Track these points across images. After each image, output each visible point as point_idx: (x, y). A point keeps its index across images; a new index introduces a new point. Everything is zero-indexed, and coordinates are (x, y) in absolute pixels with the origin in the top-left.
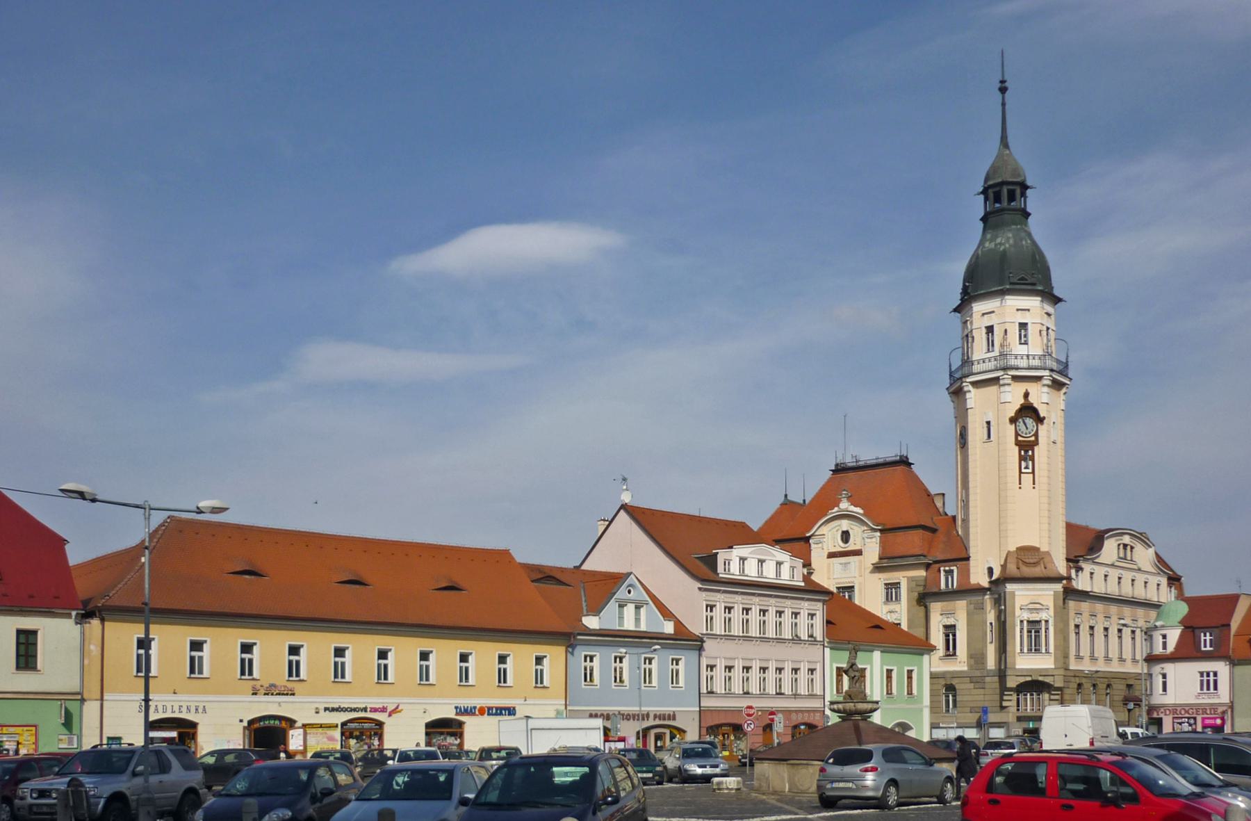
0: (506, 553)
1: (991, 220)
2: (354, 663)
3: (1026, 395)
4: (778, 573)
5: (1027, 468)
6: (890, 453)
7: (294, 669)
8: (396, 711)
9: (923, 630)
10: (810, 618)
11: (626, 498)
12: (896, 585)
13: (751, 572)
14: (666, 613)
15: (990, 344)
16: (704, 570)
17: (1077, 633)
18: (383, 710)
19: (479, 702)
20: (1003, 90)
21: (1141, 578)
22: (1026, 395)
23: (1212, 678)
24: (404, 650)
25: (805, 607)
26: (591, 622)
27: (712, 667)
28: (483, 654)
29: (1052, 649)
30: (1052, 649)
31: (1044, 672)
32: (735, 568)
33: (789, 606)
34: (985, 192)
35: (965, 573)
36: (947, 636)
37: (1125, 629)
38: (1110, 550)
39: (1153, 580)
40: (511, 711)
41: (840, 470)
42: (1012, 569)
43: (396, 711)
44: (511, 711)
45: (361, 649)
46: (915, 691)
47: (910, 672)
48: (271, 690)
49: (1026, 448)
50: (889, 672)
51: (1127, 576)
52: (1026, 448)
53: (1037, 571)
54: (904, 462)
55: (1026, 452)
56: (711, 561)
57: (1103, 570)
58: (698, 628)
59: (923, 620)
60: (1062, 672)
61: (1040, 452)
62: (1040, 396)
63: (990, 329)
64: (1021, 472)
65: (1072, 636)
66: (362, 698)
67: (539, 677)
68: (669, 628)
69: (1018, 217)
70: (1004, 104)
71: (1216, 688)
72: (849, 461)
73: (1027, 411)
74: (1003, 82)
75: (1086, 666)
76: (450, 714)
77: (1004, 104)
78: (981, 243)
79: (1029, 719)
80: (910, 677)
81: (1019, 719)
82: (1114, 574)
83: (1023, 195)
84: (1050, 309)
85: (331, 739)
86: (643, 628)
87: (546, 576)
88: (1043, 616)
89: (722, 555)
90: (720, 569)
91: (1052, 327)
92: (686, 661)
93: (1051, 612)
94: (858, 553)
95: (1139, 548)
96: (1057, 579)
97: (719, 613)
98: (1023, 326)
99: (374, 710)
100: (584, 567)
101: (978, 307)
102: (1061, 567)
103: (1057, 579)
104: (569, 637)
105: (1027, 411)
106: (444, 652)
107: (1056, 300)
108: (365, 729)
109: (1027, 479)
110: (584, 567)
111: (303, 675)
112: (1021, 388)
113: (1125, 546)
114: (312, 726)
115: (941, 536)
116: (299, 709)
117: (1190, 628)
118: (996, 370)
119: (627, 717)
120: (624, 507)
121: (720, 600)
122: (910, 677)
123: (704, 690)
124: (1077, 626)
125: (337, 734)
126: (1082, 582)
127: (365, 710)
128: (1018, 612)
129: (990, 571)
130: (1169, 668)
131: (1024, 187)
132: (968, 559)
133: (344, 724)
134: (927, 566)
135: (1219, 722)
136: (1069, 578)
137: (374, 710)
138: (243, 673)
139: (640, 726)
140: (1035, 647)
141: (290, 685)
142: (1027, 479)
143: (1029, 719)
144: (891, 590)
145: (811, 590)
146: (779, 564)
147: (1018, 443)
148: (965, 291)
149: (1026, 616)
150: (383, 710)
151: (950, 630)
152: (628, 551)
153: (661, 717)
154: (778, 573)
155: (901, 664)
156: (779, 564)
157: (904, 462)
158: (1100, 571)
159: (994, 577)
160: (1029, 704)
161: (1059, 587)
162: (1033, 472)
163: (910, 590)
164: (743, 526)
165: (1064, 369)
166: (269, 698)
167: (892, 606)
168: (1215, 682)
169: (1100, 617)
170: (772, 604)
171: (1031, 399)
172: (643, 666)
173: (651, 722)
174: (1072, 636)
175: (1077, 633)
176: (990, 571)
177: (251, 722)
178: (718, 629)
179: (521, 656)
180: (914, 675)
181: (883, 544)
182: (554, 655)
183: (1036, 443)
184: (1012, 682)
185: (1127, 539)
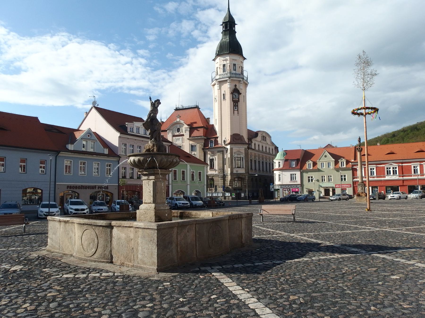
0: (36, 119)
5: (236, 109)
6: (193, 105)
22: (236, 86)
23: (294, 176)
29: (244, 167)
30: (244, 167)
41: (177, 109)
47: (200, 173)
54: (197, 107)
60: (247, 174)
64: (234, 110)
68: (106, 151)
71: (295, 179)
72: (180, 107)
78: (222, 39)
88: (242, 156)
93: (244, 155)
94: (183, 135)
96: (246, 144)
102: (246, 140)
109: (236, 112)
113: (264, 136)
118: (226, 77)
123: (121, 177)
129: (225, 141)
135: (297, 190)
139: (90, 192)
142: (236, 112)
149: (236, 156)
151: (212, 161)
157: (197, 107)
159: (226, 143)
160: (2, 316)
168: (295, 177)
171: (237, 87)
172: (80, 166)
173: (97, 190)
176: (225, 141)
183: (239, 101)
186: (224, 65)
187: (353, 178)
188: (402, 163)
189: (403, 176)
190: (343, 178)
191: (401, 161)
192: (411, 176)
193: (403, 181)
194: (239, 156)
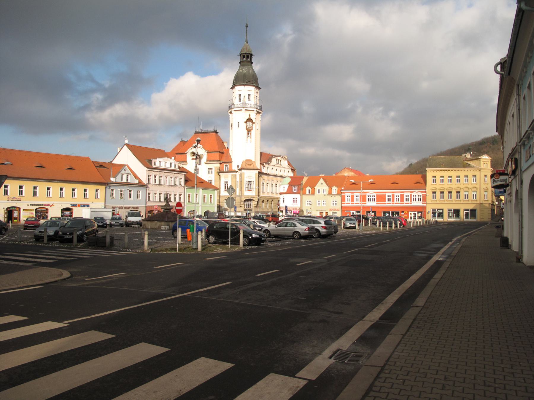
0: (88, 158)
1: (242, 63)
2: (25, 191)
3: (250, 115)
4: (171, 166)
6: (211, 129)
7: (21, 193)
8: (52, 205)
9: (218, 183)
10: (181, 178)
11: (126, 142)
12: (211, 169)
13: (163, 166)
14: (136, 177)
15: (240, 100)
16: (149, 165)
18: (49, 205)
19: (78, 203)
20: (247, 26)
21: (283, 169)
22: (250, 115)
24: (55, 187)
25: (179, 176)
26: (113, 179)
27: (150, 193)
28: (80, 189)
31: (252, 196)
32: (157, 165)
33: (174, 175)
34: (240, 55)
35: (231, 167)
37: (17, 195)
38: (274, 160)
39: (287, 170)
40: (88, 206)
42: (244, 167)
43: (52, 205)
44: (88, 206)
45: (42, 187)
46: (212, 201)
48: (14, 199)
49: (249, 131)
50: (204, 195)
51: (279, 169)
52: (249, 131)
53: (251, 167)
56: (151, 162)
57: (271, 167)
58: (145, 181)
59: (218, 180)
61: (253, 132)
62: (253, 116)
63: (240, 95)
65: (261, 186)
66: (41, 200)
67: (97, 196)
68: (137, 182)
69: (249, 64)
73: (249, 120)
75: (266, 195)
76: (69, 206)
78: (239, 70)
79: (249, 210)
80: (211, 197)
81: (245, 210)
82: (275, 168)
83: (251, 57)
84: (258, 91)
85: (32, 214)
86: (129, 181)
87: (100, 166)
89: (154, 160)
90: (153, 164)
91: (258, 96)
92: (142, 193)
95: (283, 160)
96: (258, 169)
97: (152, 178)
98: (249, 95)
99: (46, 205)
100: (113, 162)
103: (258, 169)
104: (106, 184)
105: (249, 120)
106: (68, 188)
107: (259, 88)
108: (42, 212)
109: (249, 139)
110: (113, 162)
111: (24, 194)
112: (248, 113)
114: (26, 210)
115: (225, 155)
116: (22, 205)
117: (291, 184)
119: (121, 208)
120: (126, 144)
121: (153, 173)
122: (211, 197)
125: (34, 212)
126: (264, 170)
127: (43, 205)
129: (238, 166)
130: (285, 196)
131: (251, 55)
132: (232, 162)
133: (36, 209)
134: (221, 164)
136: (260, 169)
137: (46, 205)
138: (5, 194)
140: (250, 189)
141: (20, 198)
142: (249, 139)
143: (249, 210)
144: (210, 170)
145: (182, 171)
146: (171, 163)
147: (247, 129)
148: (234, 84)
150: (49, 205)
152: (125, 157)
153: (134, 208)
154: (171, 166)
155: (208, 193)
156: (171, 163)
157: (216, 132)
158: (270, 167)
161: (257, 172)
163: (215, 171)
164: (162, 151)
165: (261, 108)
166: (13, 201)
167: (210, 175)
169: (271, 180)
170: (169, 175)
174: (261, 186)
176: (238, 166)
177: (7, 209)
178: (152, 182)
179: (90, 189)
180: (212, 197)
181: (208, 156)
182: (101, 189)
183: (252, 129)
184: (243, 199)
185: (279, 158)
190: (335, 203)
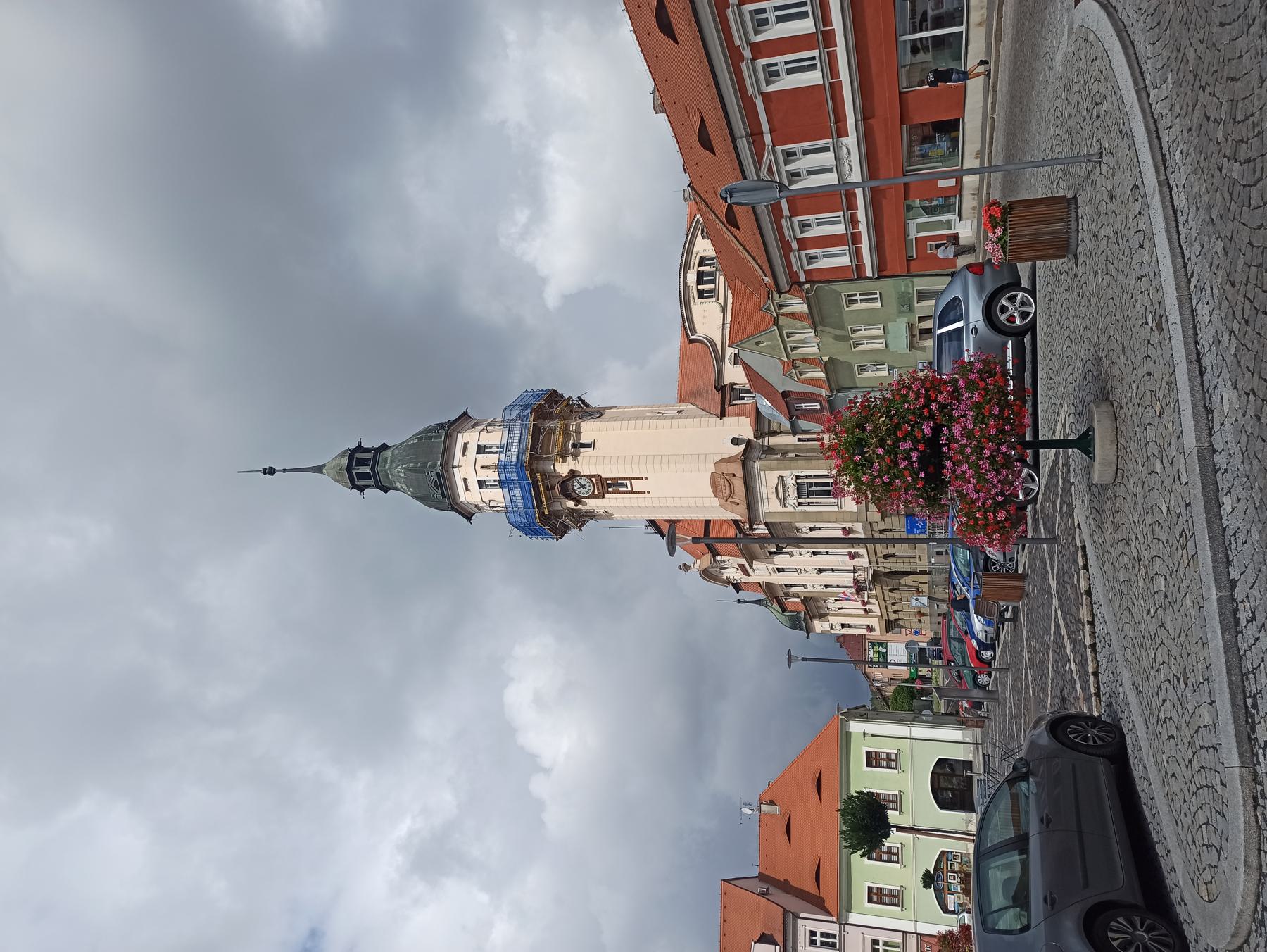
17: (849, 626)
20: (272, 471)
36: (811, 494)
55: (609, 486)
64: (632, 492)
70: (284, 471)
74: (264, 471)
77: (284, 471)
88: (790, 482)
101: (463, 496)
109: (637, 486)
124: (843, 626)
128: (790, 509)
142: (637, 486)
149: (792, 500)
162: (630, 479)
175: (849, 626)
186: (481, 450)
187: (861, 276)
188: (755, 134)
189: (840, 118)
191: (743, 144)
192: (835, 88)
193: (866, 118)
194: (793, 492)
